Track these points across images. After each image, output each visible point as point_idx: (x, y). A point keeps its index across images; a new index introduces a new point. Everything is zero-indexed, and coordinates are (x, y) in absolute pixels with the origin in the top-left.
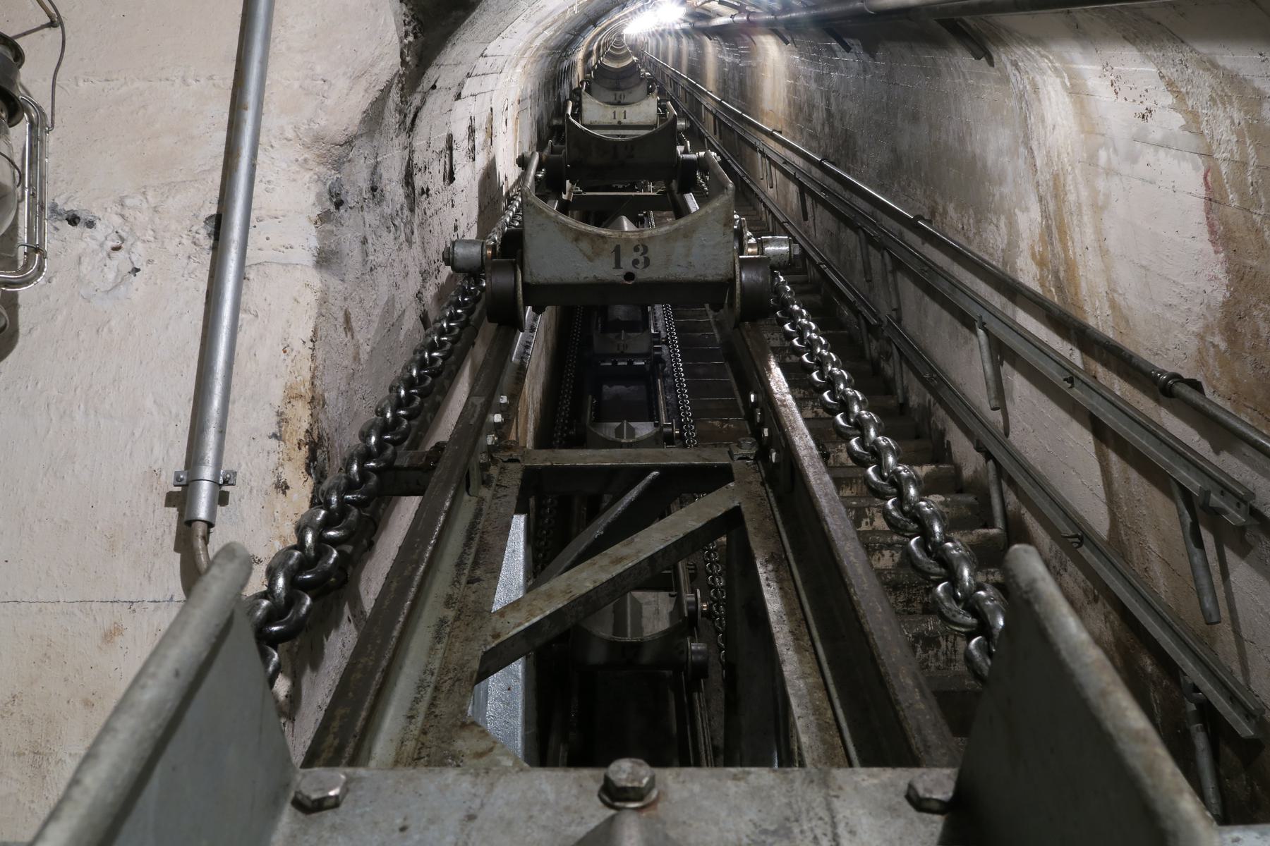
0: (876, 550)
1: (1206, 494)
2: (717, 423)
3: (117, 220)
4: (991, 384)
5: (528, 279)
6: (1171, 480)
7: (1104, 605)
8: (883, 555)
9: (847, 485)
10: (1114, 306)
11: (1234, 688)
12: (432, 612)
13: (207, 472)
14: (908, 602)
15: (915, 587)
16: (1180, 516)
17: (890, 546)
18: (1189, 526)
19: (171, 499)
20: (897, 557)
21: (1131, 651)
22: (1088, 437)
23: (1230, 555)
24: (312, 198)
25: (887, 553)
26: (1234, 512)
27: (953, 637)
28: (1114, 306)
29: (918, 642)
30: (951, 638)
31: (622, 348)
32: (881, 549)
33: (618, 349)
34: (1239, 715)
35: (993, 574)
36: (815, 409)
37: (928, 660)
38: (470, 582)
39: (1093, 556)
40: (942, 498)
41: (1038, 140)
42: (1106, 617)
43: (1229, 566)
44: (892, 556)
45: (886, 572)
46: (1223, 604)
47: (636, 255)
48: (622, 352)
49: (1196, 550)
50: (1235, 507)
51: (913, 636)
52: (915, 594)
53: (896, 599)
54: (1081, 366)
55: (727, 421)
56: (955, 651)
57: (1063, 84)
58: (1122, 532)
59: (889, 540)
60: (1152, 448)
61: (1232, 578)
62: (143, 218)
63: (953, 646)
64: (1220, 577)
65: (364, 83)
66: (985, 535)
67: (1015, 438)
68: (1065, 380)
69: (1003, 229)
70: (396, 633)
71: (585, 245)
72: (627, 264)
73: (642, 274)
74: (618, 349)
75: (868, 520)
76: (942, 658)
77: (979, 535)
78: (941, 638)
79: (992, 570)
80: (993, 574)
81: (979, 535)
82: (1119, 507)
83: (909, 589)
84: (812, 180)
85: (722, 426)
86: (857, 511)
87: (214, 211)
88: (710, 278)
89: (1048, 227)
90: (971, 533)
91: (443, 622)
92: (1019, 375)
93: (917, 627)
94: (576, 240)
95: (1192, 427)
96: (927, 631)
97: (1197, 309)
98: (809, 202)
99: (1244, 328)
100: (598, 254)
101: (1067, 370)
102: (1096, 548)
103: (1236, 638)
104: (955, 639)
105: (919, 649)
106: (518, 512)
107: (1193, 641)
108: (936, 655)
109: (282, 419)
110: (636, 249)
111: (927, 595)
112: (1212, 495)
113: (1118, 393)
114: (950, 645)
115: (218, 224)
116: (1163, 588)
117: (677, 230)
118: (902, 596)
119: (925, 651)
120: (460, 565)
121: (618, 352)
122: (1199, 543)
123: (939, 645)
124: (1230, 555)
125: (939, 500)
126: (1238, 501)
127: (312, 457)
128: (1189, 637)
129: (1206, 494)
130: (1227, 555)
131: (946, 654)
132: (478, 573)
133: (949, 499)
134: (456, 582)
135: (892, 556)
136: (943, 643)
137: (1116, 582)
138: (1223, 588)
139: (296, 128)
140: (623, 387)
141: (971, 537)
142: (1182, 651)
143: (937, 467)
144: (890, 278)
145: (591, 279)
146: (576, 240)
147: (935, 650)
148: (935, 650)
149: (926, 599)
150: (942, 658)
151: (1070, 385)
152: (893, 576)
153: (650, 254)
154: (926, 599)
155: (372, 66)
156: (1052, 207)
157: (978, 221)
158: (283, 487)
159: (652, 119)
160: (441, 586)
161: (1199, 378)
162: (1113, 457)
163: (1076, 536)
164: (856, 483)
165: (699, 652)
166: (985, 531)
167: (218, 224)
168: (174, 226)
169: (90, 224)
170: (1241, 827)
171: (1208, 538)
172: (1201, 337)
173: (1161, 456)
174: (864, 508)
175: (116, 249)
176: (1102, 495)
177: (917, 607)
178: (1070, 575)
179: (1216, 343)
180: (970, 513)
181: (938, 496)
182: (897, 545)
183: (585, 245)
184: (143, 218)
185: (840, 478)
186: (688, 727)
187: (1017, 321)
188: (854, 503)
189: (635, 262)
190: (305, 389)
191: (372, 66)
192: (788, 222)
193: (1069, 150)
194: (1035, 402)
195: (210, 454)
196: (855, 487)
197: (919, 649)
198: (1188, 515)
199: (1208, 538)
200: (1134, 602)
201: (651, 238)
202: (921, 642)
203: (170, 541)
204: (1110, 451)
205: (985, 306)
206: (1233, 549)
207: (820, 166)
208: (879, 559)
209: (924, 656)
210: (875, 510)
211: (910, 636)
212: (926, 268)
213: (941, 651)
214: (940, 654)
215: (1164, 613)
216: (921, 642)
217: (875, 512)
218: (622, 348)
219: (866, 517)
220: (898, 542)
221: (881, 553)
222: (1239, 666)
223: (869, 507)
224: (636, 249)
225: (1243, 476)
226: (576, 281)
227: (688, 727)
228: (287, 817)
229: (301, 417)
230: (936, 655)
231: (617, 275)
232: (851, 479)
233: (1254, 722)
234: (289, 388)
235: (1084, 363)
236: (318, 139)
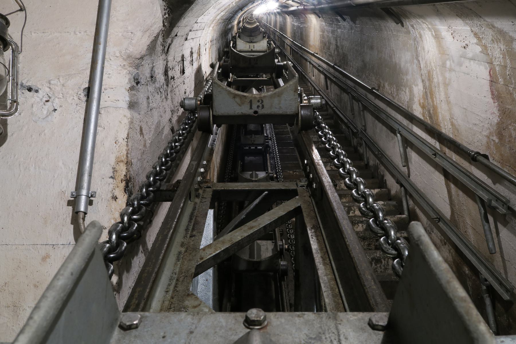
0: (356, 224)
1: (490, 201)
2: (291, 172)
3: (48, 90)
4: (403, 156)
5: (215, 114)
6: (476, 195)
7: (449, 246)
8: (359, 226)
9: (344, 197)
10: (452, 124)
11: (502, 280)
12: (175, 249)
13: (84, 192)
14: (369, 245)
15: (372, 239)
16: (479, 210)
17: (362, 222)
18: (483, 214)
19: (69, 203)
20: (365, 226)
21: (460, 265)
22: (442, 178)
23: (500, 226)
24: (127, 80)
25: (360, 225)
26: (501, 208)
27: (387, 259)
28: (452, 124)
29: (373, 261)
30: (386, 259)
31: (253, 142)
32: (358, 223)
33: (251, 142)
34: (503, 291)
35: (403, 233)
36: (331, 166)
37: (377, 268)
38: (191, 236)
39: (444, 226)
40: (383, 203)
41: (422, 57)
42: (449, 251)
43: (499, 230)
44: (363, 226)
45: (360, 233)
46: (497, 246)
47: (258, 104)
48: (253, 143)
49: (486, 224)
50: (502, 206)
51: (371, 259)
52: (372, 242)
53: (364, 244)
54: (439, 149)
55: (295, 171)
56: (388, 265)
57: (432, 34)
58: (456, 216)
59: (361, 220)
60: (468, 182)
61: (501, 235)
62: (58, 88)
63: (387, 263)
64: (496, 235)
65: (148, 34)
66: (400, 218)
67: (412, 178)
68: (433, 154)
69: (408, 93)
70: (161, 258)
71: (238, 100)
72: (255, 108)
73: (261, 112)
74: (251, 142)
75: (353, 211)
76: (383, 268)
77: (398, 218)
78: (382, 260)
79: (403, 232)
80: (403, 233)
81: (398, 218)
82: (455, 206)
83: (369, 239)
84: (330, 73)
85: (293, 173)
86: (348, 208)
87: (87, 86)
88: (288, 113)
89: (426, 92)
90: (395, 217)
91: (180, 253)
92: (414, 152)
93: (373, 255)
94: (234, 97)
95: (484, 174)
96: (377, 256)
97: (486, 126)
98: (329, 82)
99: (506, 134)
100: (243, 103)
101: (434, 150)
102: (445, 223)
103: (502, 259)
104: (388, 260)
105: (373, 264)
106: (211, 208)
107: (485, 261)
108: (380, 267)
109: (115, 170)
110: (258, 101)
111: (377, 242)
112: (492, 201)
113: (454, 160)
114: (386, 262)
115: (89, 91)
116: (472, 239)
117: (275, 93)
118: (367, 242)
119: (376, 265)
120: (187, 230)
121: (251, 143)
122: (487, 221)
123: (381, 262)
124: (500, 226)
125: (381, 203)
126: (503, 204)
127: (127, 186)
128: (483, 259)
129: (490, 201)
130: (498, 226)
131: (384, 266)
132: (194, 233)
133: (386, 203)
134: (185, 236)
135: (363, 226)
136: (383, 262)
137: (454, 237)
138: (497, 239)
139: (120, 52)
140: (253, 157)
141: (394, 218)
142: (480, 265)
143: (381, 190)
144: (362, 113)
145: (240, 113)
146: (234, 97)
147: (380, 264)
148: (380, 264)
149: (376, 244)
150: (383, 268)
151: (435, 156)
152: (363, 234)
153: (264, 103)
154: (376, 244)
155: (151, 27)
156: (427, 84)
157: (397, 90)
158: (115, 198)
159: (265, 49)
160: (179, 238)
161: (487, 154)
162: (452, 186)
163: (437, 218)
164: (348, 196)
165: (284, 265)
166: (400, 216)
167: (89, 91)
168: (71, 92)
169: (37, 91)
170: (504, 336)
171: (491, 219)
172: (488, 137)
173: (472, 185)
174: (351, 206)
175: (47, 101)
176: (448, 201)
177: (373, 247)
178: (435, 234)
179: (494, 140)
180: (394, 209)
181: (381, 202)
182: (364, 222)
183: (238, 100)
184: (58, 88)
185: (341, 194)
186: (280, 296)
187: (413, 130)
188: (347, 205)
189: (258, 107)
190: (124, 158)
191: (151, 27)
192: (320, 90)
193: (435, 61)
194: (421, 163)
195: (85, 185)
196: (347, 198)
197: (373, 264)
198: (483, 210)
199: (491, 219)
200: (461, 245)
201: (265, 97)
202: (374, 261)
203: (69, 220)
204: (451, 183)
205: (400, 124)
206: (501, 223)
207: (333, 67)
208: (357, 227)
209: (375, 267)
210: (356, 207)
211: (370, 258)
212: (376, 109)
213: (382, 265)
214: (382, 266)
215: (473, 249)
216: (374, 261)
217: (355, 208)
218: (253, 142)
219: (352, 210)
220: (365, 221)
221: (358, 225)
222: (504, 271)
223: (353, 206)
224: (258, 101)
225: (505, 194)
226: (234, 114)
227: (280, 296)
228: (117, 332)
229: (122, 170)
230: (380, 267)
231: (251, 112)
232: (346, 195)
233: (509, 293)
234: (117, 158)
235: (441, 148)
236: (129, 56)
